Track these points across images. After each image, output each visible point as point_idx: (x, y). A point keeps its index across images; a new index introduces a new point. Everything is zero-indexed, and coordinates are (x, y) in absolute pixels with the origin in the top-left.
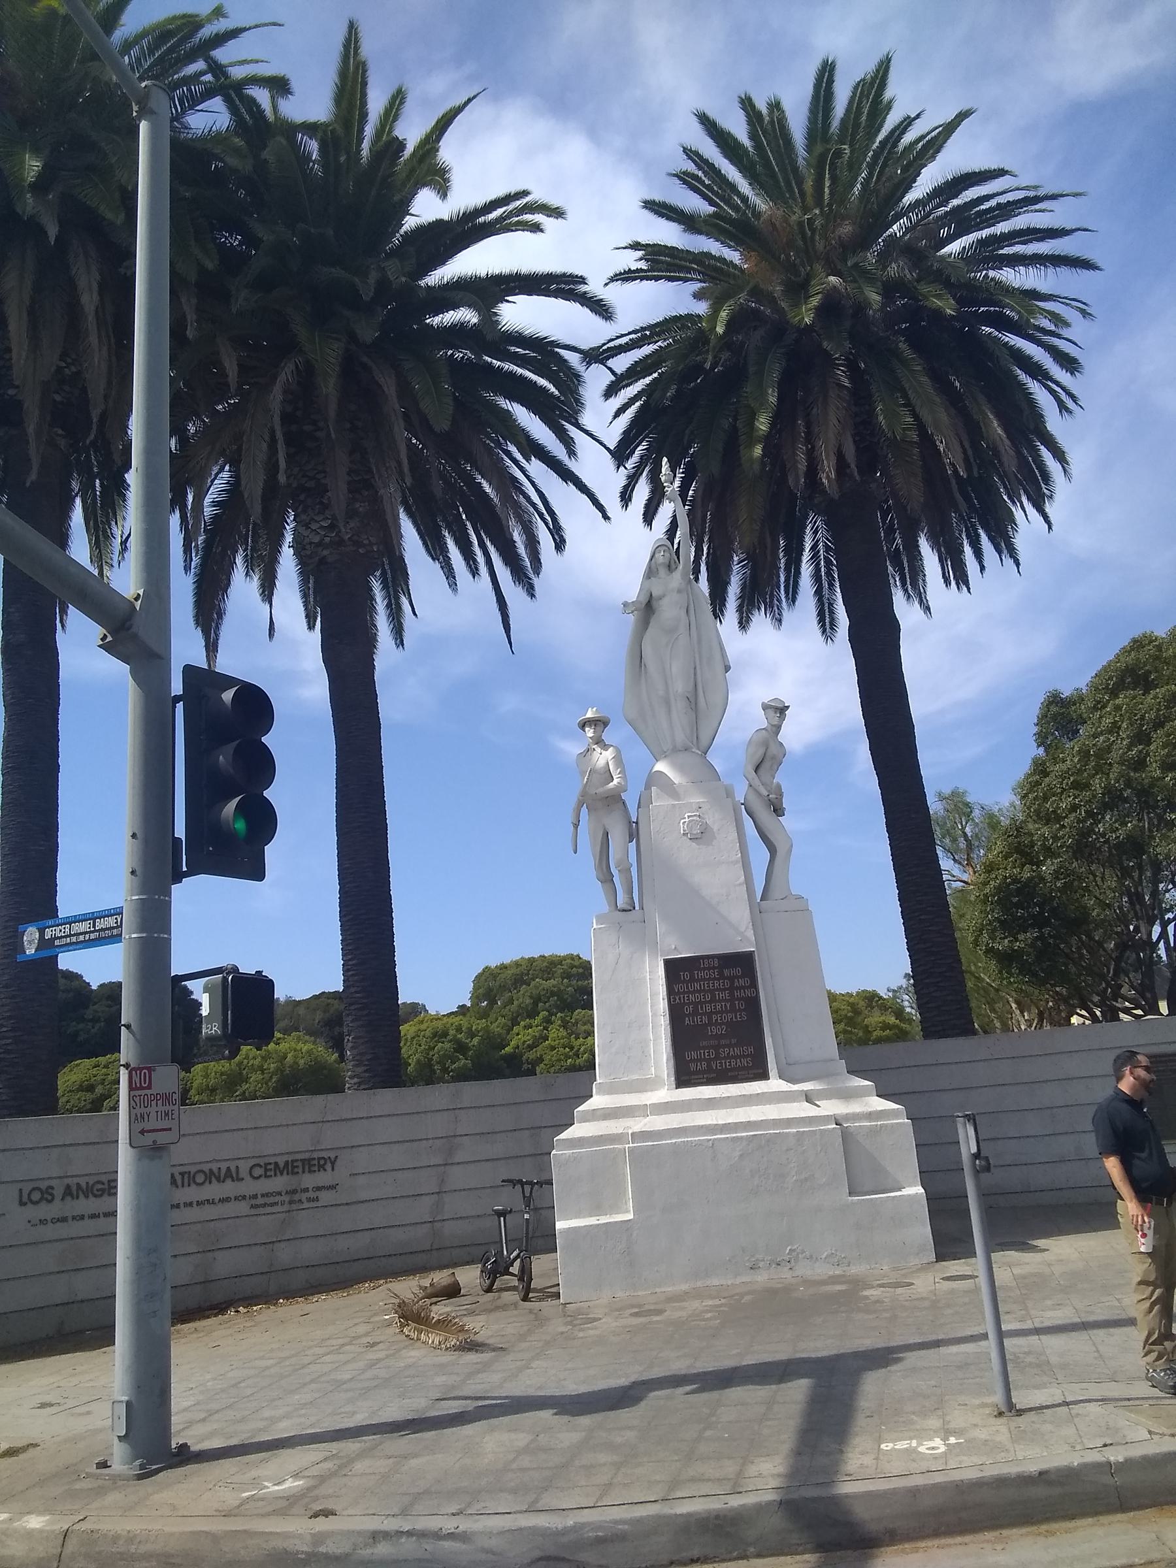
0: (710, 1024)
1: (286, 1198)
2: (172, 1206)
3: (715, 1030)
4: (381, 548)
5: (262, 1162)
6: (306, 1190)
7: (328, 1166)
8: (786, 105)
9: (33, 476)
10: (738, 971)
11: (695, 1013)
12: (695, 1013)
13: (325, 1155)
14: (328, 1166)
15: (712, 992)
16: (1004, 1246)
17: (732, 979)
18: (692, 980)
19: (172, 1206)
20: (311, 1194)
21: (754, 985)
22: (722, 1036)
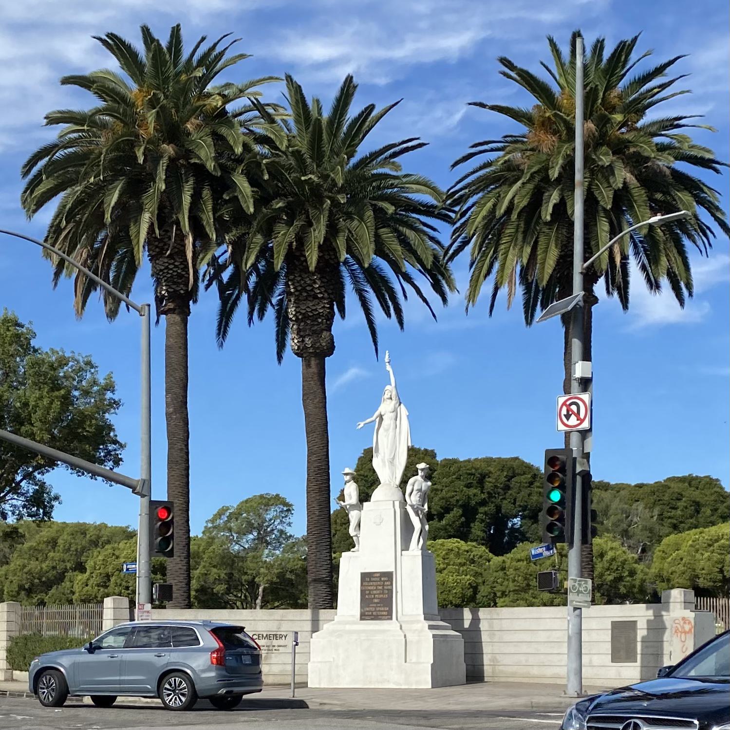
0: (374, 598)
1: (267, 648)
2: (564, 691)
3: (376, 601)
4: (332, 287)
5: (257, 633)
6: (274, 646)
7: (283, 638)
8: (340, 318)
9: (149, 686)
10: (386, 579)
11: (370, 594)
12: (370, 594)
13: (282, 633)
14: (283, 638)
15: (376, 586)
16: (483, 679)
17: (384, 581)
18: (370, 581)
19: (564, 691)
20: (276, 648)
21: (362, 591)
22: (378, 603)
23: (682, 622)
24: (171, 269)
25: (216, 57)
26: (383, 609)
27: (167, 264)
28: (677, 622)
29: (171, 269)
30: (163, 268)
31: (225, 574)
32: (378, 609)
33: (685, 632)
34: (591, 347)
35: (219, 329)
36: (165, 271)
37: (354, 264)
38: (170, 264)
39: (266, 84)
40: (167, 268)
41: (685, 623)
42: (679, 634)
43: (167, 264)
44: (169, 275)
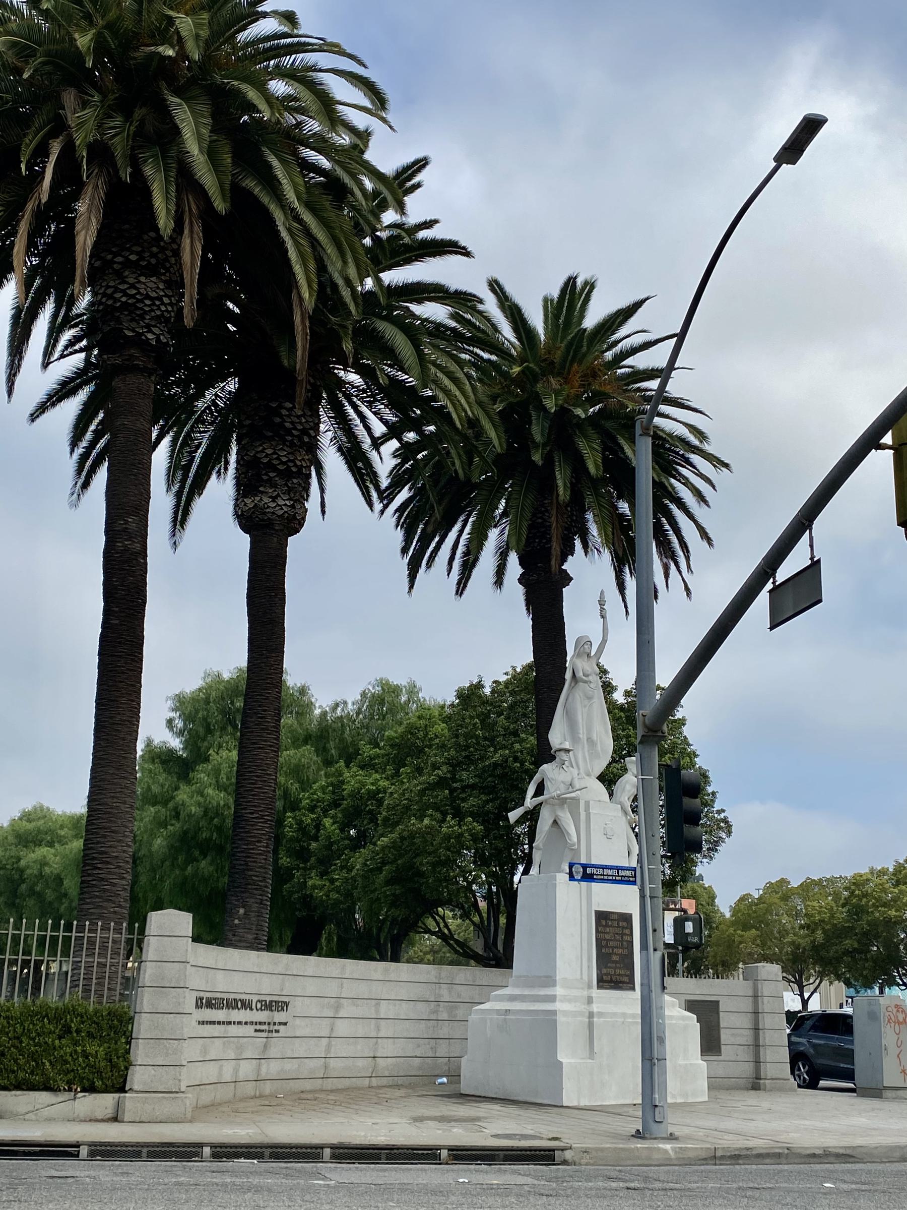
3: (615, 958)
23: (895, 1010)
24: (165, 305)
25: (367, 488)
26: (622, 972)
27: (162, 293)
28: (889, 1009)
29: (165, 305)
30: (154, 295)
31: (452, 818)
32: (618, 971)
33: (899, 1023)
34: (286, 556)
35: (176, 513)
36: (157, 303)
37: (62, 995)
38: (166, 296)
39: (496, 1108)
40: (159, 298)
41: (898, 1011)
42: (893, 1024)
43: (162, 293)
44: (158, 313)
